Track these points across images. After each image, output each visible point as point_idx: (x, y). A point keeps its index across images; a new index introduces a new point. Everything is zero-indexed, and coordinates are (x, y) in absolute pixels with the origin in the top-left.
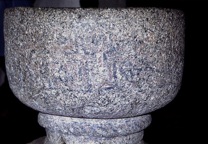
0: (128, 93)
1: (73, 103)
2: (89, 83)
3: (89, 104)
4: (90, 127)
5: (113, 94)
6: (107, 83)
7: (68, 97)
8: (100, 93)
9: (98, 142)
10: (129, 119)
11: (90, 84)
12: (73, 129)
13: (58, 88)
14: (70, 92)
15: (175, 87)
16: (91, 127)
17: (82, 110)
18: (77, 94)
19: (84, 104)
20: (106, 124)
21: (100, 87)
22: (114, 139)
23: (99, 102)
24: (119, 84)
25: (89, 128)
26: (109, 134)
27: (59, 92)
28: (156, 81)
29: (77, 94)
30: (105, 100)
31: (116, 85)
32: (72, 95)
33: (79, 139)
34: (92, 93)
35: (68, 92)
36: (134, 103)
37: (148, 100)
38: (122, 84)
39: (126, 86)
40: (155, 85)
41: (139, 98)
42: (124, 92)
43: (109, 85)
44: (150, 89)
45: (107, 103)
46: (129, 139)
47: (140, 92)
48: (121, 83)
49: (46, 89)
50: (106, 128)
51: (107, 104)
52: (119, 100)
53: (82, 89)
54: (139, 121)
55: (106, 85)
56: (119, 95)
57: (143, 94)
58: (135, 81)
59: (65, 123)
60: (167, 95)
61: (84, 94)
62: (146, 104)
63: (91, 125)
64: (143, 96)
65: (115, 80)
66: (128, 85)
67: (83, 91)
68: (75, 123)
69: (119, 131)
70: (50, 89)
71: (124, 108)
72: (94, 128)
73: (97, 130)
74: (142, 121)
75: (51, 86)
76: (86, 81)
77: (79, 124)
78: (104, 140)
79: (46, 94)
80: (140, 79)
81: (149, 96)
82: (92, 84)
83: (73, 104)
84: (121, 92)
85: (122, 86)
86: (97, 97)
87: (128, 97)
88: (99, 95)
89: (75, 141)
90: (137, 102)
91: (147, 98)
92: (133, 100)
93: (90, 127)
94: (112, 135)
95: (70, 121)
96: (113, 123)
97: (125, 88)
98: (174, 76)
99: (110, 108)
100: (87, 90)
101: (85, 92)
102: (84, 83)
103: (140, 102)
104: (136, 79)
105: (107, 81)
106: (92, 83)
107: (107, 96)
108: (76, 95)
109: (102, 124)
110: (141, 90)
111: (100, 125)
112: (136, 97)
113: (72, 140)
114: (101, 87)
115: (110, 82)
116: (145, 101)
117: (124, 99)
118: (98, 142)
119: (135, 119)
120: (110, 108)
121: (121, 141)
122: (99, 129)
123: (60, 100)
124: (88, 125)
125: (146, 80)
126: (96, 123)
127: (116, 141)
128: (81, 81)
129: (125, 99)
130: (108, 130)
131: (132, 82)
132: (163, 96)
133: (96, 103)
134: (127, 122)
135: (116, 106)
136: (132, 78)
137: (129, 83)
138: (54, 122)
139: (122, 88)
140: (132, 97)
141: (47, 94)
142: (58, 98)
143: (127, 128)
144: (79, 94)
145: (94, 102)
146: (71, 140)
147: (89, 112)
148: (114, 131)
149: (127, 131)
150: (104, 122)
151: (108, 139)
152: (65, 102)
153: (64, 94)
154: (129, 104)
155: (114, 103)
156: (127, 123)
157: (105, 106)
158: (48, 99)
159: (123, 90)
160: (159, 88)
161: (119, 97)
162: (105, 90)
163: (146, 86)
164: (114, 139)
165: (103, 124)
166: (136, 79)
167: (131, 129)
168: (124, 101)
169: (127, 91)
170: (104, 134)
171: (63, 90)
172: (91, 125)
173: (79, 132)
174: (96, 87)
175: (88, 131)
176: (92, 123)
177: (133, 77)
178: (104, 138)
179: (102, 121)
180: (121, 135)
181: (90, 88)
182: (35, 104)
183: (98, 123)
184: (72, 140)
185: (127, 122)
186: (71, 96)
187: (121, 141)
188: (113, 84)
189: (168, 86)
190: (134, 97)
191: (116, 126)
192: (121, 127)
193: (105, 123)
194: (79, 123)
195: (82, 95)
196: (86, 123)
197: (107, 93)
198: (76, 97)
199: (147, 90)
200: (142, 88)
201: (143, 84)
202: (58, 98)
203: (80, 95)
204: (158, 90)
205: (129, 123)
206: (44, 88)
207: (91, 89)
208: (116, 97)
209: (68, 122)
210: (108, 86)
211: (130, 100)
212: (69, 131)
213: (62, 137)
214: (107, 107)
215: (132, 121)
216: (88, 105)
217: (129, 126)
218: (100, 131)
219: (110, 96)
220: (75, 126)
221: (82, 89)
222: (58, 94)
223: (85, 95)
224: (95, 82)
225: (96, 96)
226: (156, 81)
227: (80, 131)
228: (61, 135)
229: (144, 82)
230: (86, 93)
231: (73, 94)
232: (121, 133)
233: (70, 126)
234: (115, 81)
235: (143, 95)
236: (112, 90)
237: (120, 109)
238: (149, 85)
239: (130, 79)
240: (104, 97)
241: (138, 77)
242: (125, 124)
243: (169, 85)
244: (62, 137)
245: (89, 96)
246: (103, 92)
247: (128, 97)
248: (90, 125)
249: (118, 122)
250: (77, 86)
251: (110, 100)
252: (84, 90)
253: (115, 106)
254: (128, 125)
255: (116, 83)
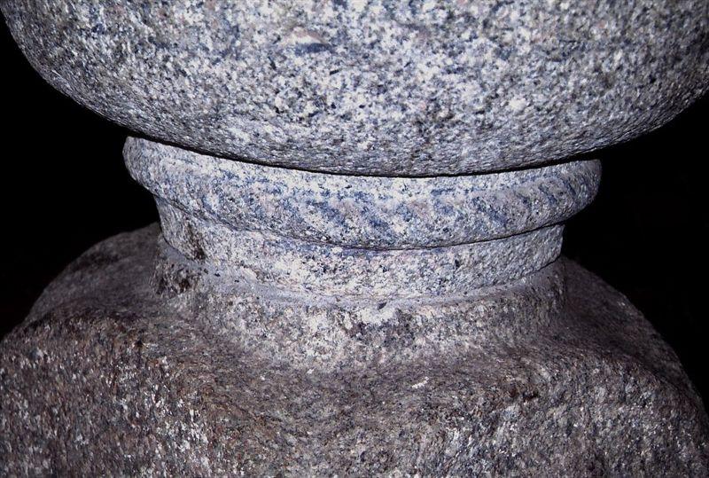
0: (398, 73)
1: (175, 96)
2: (229, 18)
3: (239, 108)
4: (278, 197)
5: (332, 73)
6: (302, 26)
7: (155, 71)
8: (277, 65)
9: (315, 264)
10: (446, 180)
11: (233, 24)
12: (217, 201)
13: (121, 29)
14: (161, 50)
15: (648, 59)
16: (282, 201)
17: (219, 127)
18: (186, 60)
19: (221, 107)
20: (346, 196)
21: (275, 38)
22: (385, 257)
23: (278, 102)
24: (354, 34)
25: (277, 204)
26: (353, 234)
27: (123, 45)
28: (531, 30)
29: (186, 60)
30: (300, 94)
31: (344, 34)
32: (169, 65)
33: (247, 240)
34: (243, 65)
35: (154, 50)
36: (431, 119)
37: (494, 110)
38: (370, 36)
39: (387, 42)
40: (526, 49)
41: (451, 99)
42: (381, 67)
43: (313, 33)
44: (499, 62)
45: (310, 108)
46: (458, 264)
47: (453, 75)
48: (365, 27)
49: (81, 29)
50: (342, 210)
51: (311, 115)
52: (361, 101)
53: (202, 41)
54: (501, 196)
55: (299, 35)
56: (357, 82)
57: (464, 81)
58: (428, 23)
59: (195, 173)
60: (602, 94)
61: (214, 64)
62: (491, 126)
63: (286, 193)
64: (469, 92)
65: (337, 13)
66: (394, 40)
67: (206, 49)
68: (226, 177)
69: (398, 229)
70: (94, 30)
71: (389, 138)
72: (294, 205)
73: (303, 210)
74: (520, 196)
75: (96, 17)
76: (217, 9)
77: (240, 183)
78: (340, 255)
79: (82, 49)
80: (451, 17)
81: (497, 96)
82: (243, 26)
83: (178, 102)
84: (366, 67)
85: (368, 41)
86: (268, 83)
87: (398, 90)
88: (275, 72)
89: (232, 249)
90: (442, 114)
91: (489, 106)
92: (422, 104)
93: (278, 197)
94: (364, 239)
95: (211, 167)
96: (373, 191)
97: (382, 52)
98: (645, 9)
99: (324, 129)
100: (222, 47)
101: (215, 57)
102: (212, 19)
103: (458, 116)
104: (434, 17)
105: (303, 16)
106: (240, 19)
107: (307, 80)
108: (183, 65)
109: (328, 193)
110: (456, 66)
111: (322, 194)
112: (433, 94)
113: (224, 243)
114: (279, 39)
115: (317, 20)
116: (482, 112)
117: (382, 98)
118: (315, 264)
119: (482, 185)
120: (327, 130)
121: (414, 267)
122: (311, 212)
123: (131, 82)
124: (275, 192)
125: (481, 21)
126: (303, 185)
127: (393, 266)
128: (199, 10)
129: (389, 100)
130: (351, 219)
131: (411, 27)
132: (574, 96)
133: (266, 107)
134: (440, 192)
135: (349, 123)
136: (414, 12)
137: (399, 31)
138: (161, 164)
139: (367, 51)
140: (419, 93)
141: (86, 50)
142: (123, 70)
143: (435, 217)
144: (195, 63)
145: (255, 99)
146: (220, 241)
147: (248, 140)
148: (375, 224)
149: (431, 229)
150: (335, 183)
151: (358, 256)
152: (147, 91)
153: (140, 58)
154: (404, 121)
155: (342, 113)
156: (440, 197)
157: (304, 123)
158: (92, 71)
159: (376, 60)
160: (548, 60)
161: (359, 89)
162: (298, 53)
163: (482, 49)
164: (385, 257)
165: (332, 192)
166: (434, 17)
167: (451, 224)
168: (384, 108)
169: (390, 63)
170: (331, 234)
171: (136, 42)
172: (285, 191)
173: (240, 216)
174: (256, 37)
175: (270, 214)
176: (291, 184)
177: (418, 6)
178: (338, 250)
179: (327, 179)
180: (405, 243)
181: (233, 42)
182: (133, 91)
183: (314, 185)
184: (224, 243)
185: (440, 192)
186: (165, 67)
187: (414, 267)
188: (328, 30)
189: (603, 54)
190: (427, 95)
191: (389, 205)
192: (405, 211)
193: (340, 189)
194: (243, 179)
195: (205, 68)
196: (265, 180)
197: (306, 68)
198: (184, 74)
199: (488, 67)
200: (463, 58)
201: (467, 38)
202: (121, 71)
203: (196, 66)
204: (542, 70)
205: (447, 198)
206: (71, 23)
207: (238, 43)
208: (344, 86)
209: (204, 171)
210: (308, 40)
211: (411, 106)
212: (204, 205)
213: (190, 226)
214: (310, 125)
215: (462, 192)
216: (235, 111)
217: (447, 210)
218: (317, 221)
219: (320, 82)
220: (225, 190)
221: (202, 41)
222: (120, 56)
223: (218, 70)
224: (252, 19)
225: (261, 76)
226: (531, 30)
227: (241, 211)
228: (187, 219)
229: (473, 32)
230: (218, 60)
231: (171, 59)
232: (405, 237)
233: (207, 186)
234: (339, 17)
235: (469, 86)
236: (326, 54)
237: (371, 138)
238: (495, 46)
239: (405, 16)
240: (296, 86)
241: (443, 8)
242: (429, 202)
243: (613, 50)
244: (190, 226)
245: (234, 75)
246: (286, 62)
247: (398, 90)
248: (280, 192)
249: (396, 191)
250: (183, 27)
251: (321, 98)
252: (211, 49)
253: (345, 126)
254: (441, 206)
255: (341, 27)
